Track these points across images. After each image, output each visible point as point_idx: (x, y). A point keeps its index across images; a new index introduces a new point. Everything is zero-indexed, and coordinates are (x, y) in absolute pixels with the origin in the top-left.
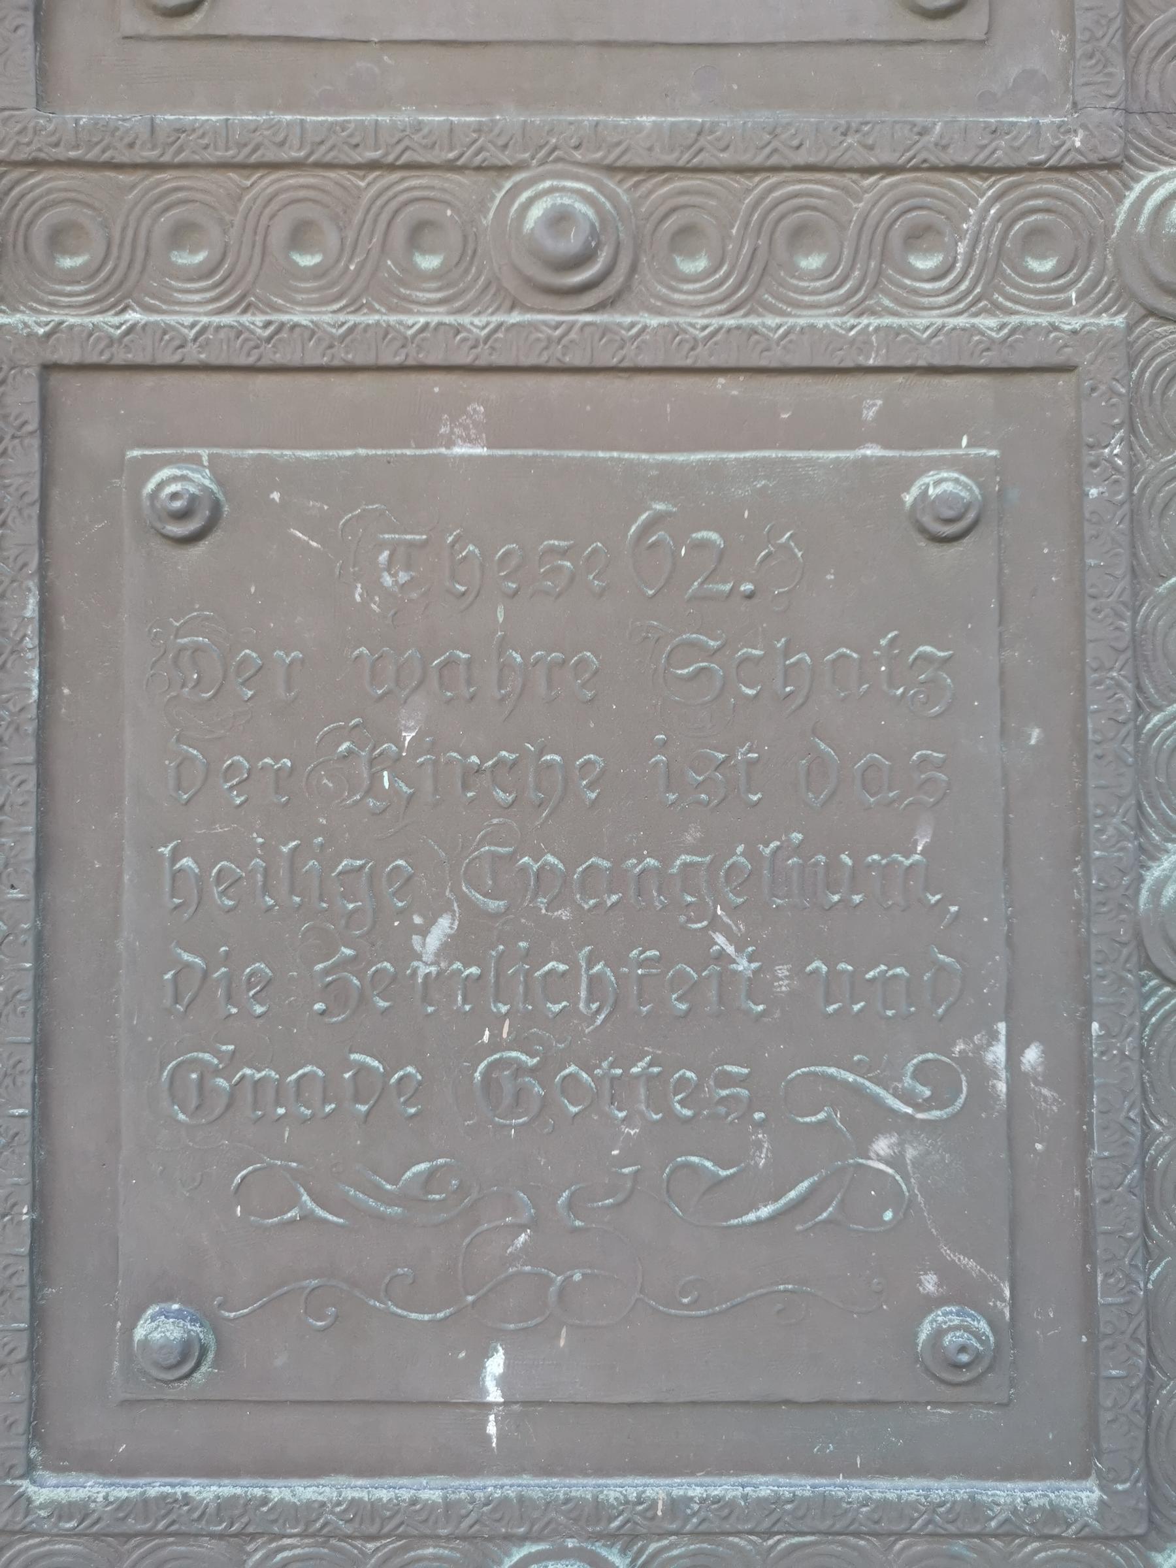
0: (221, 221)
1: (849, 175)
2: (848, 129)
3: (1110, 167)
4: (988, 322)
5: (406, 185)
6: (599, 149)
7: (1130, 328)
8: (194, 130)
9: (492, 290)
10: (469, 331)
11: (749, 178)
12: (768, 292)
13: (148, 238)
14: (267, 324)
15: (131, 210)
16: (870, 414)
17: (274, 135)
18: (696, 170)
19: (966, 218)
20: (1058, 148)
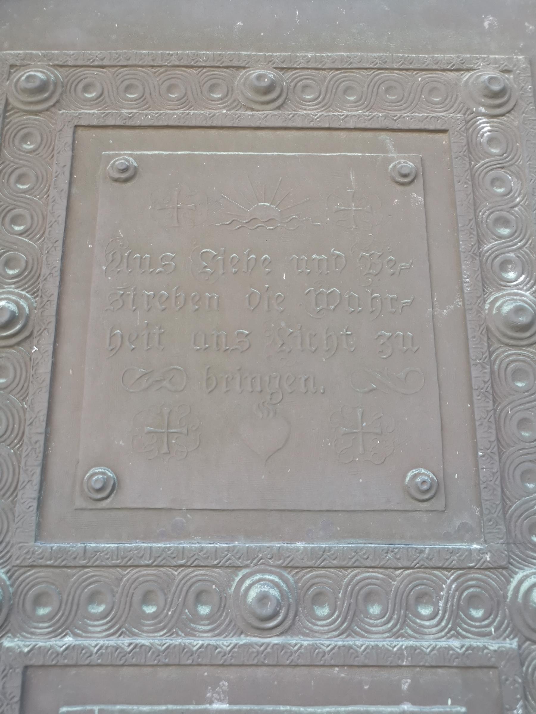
0: (112, 591)
1: (389, 570)
2: (388, 550)
3: (504, 568)
4: (455, 643)
5: (195, 573)
6: (280, 559)
7: (520, 646)
8: (103, 551)
9: (233, 624)
10: (221, 648)
11: (346, 570)
12: (356, 625)
13: (79, 600)
14: (130, 644)
15: (72, 587)
16: (405, 687)
17: (139, 553)
18: (323, 567)
19: (442, 589)
20: (480, 560)
